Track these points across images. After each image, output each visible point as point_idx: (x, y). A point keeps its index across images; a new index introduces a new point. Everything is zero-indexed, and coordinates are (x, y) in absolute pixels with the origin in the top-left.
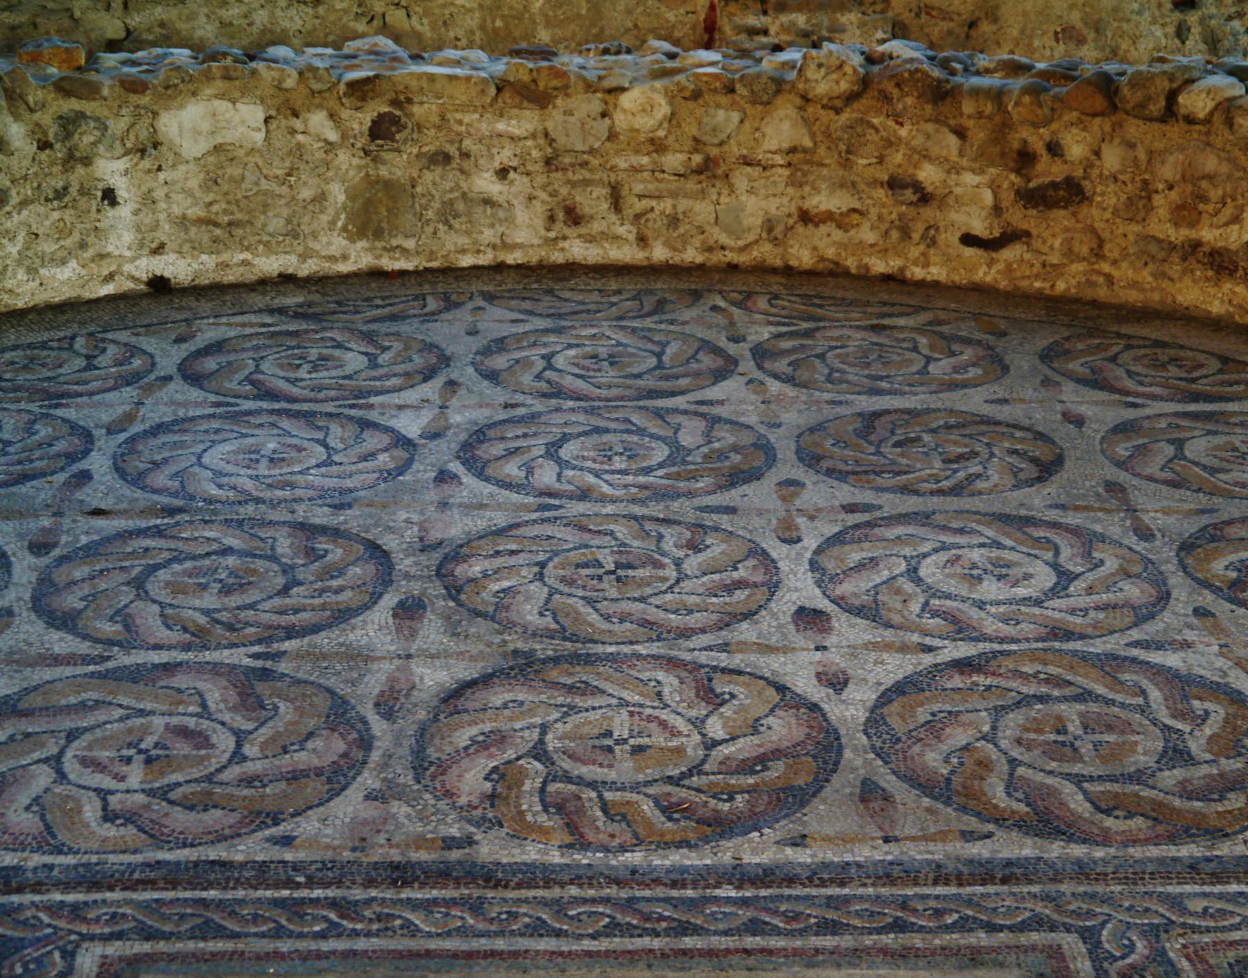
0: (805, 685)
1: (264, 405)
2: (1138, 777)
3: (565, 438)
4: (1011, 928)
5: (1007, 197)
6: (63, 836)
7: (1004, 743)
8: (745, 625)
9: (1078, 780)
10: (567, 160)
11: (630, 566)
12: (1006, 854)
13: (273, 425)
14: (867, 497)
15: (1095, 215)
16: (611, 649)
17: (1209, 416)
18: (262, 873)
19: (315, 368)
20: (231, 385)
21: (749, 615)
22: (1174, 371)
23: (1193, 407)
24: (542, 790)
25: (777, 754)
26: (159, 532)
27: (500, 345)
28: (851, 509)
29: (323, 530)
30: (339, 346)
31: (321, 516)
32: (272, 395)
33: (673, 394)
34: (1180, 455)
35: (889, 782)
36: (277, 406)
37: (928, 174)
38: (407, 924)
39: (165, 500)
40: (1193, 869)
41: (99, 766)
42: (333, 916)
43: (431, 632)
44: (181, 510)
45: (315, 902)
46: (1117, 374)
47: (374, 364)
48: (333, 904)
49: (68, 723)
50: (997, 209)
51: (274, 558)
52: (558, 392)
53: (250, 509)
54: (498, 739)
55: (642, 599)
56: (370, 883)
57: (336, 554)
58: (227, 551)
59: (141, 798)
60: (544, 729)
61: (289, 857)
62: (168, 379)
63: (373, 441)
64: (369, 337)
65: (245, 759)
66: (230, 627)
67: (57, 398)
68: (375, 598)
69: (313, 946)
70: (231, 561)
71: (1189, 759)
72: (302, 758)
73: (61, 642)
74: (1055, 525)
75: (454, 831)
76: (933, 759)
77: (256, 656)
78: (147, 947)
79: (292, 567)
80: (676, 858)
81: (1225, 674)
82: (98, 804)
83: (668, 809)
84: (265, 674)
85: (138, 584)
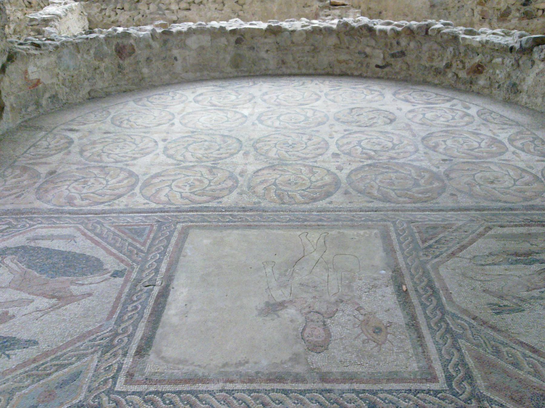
0: (333, 170)
1: (213, 108)
2: (408, 190)
3: (281, 115)
4: (377, 221)
5: (387, 55)
6: (173, 202)
7: (377, 182)
8: (320, 157)
9: (394, 190)
10: (282, 48)
11: (295, 144)
12: (376, 206)
13: (215, 112)
14: (350, 128)
15: (407, 59)
16: (291, 162)
17: (432, 108)
18: (215, 209)
19: (224, 99)
20: (205, 103)
21: (321, 155)
22: (424, 97)
23: (428, 106)
24: (275, 192)
25: (326, 185)
26: (190, 137)
27: (266, 93)
28: (345, 130)
29: (227, 136)
30: (229, 94)
31: (226, 133)
32: (215, 106)
33: (306, 104)
34: (424, 117)
35: (351, 190)
36: (215, 108)
37: (368, 50)
38: (246, 219)
39: (191, 129)
40: (419, 210)
41: (179, 187)
42: (231, 218)
43: (251, 159)
44: (195, 132)
45: (227, 215)
46: (410, 98)
47: (237, 98)
48: (231, 215)
49: (172, 178)
50: (384, 58)
51: (216, 142)
52: (279, 105)
53: (210, 132)
54: (265, 181)
55: (298, 151)
56: (238, 211)
57: (230, 142)
58: (206, 141)
59: (189, 194)
60: (276, 179)
61: (221, 206)
62: (191, 102)
63: (238, 116)
64: (237, 92)
65: (211, 186)
66: (207, 158)
67: (166, 106)
68: (239, 151)
69: (227, 224)
70: (206, 143)
71: (419, 185)
72: (224, 185)
73: (170, 161)
74: (393, 133)
75: (256, 200)
76: (361, 186)
77: (213, 164)
78: (192, 224)
79: (220, 144)
80: (304, 206)
81: (430, 167)
82: (180, 195)
83: (302, 196)
84: (214, 168)
85: (186, 148)
